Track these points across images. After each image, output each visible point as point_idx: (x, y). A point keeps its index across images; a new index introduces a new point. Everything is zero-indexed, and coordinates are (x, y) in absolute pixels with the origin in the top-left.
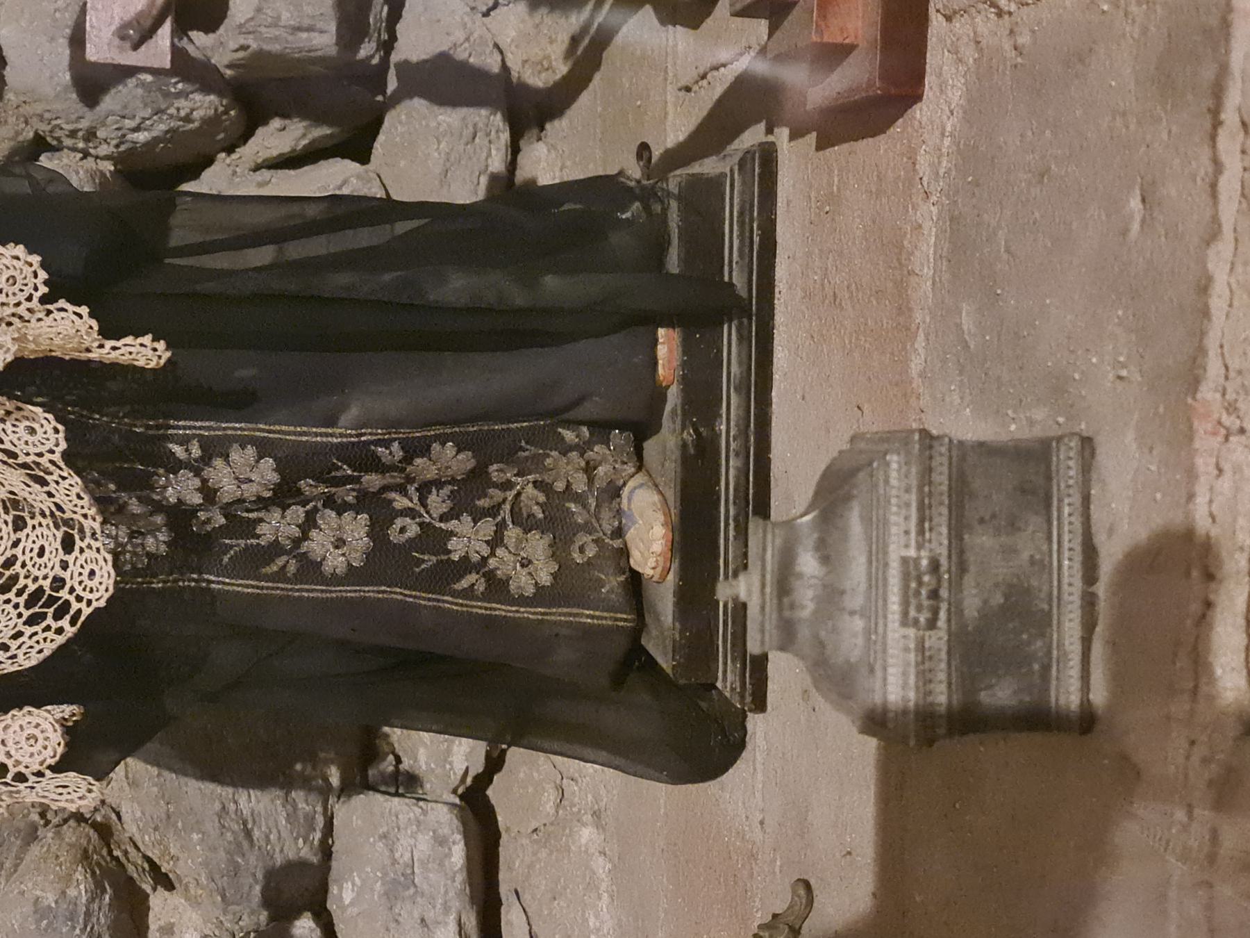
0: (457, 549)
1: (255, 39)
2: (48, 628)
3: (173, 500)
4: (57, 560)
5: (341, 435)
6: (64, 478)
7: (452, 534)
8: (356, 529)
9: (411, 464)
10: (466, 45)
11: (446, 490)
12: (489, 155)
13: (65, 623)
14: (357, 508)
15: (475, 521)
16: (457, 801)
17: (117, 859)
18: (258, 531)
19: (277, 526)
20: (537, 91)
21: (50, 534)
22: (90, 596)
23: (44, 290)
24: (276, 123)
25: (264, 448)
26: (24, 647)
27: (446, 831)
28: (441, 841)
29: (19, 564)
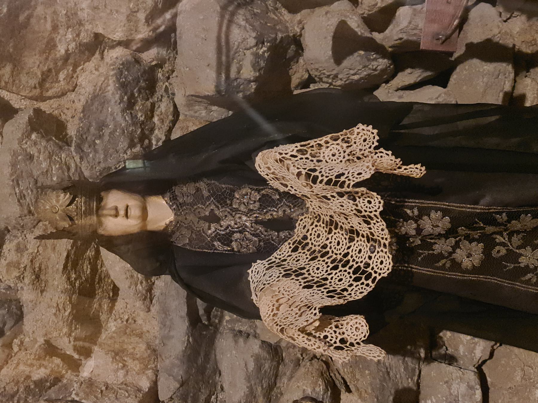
0: (523, 261)
1: (406, 35)
2: (363, 284)
3: (404, 233)
4: (367, 256)
5: (481, 209)
6: (378, 222)
7: (521, 255)
8: (477, 249)
9: (510, 223)
10: (499, 35)
11: (520, 236)
12: (505, 83)
13: (370, 282)
14: (479, 241)
15: (533, 250)
16: (476, 370)
17: (331, 377)
18: (433, 248)
19: (442, 247)
20: (527, 54)
21: (365, 245)
22: (380, 272)
23: (376, 144)
24: (409, 70)
25: (445, 212)
26: (354, 290)
27: (473, 383)
28: (471, 388)
29: (350, 256)
